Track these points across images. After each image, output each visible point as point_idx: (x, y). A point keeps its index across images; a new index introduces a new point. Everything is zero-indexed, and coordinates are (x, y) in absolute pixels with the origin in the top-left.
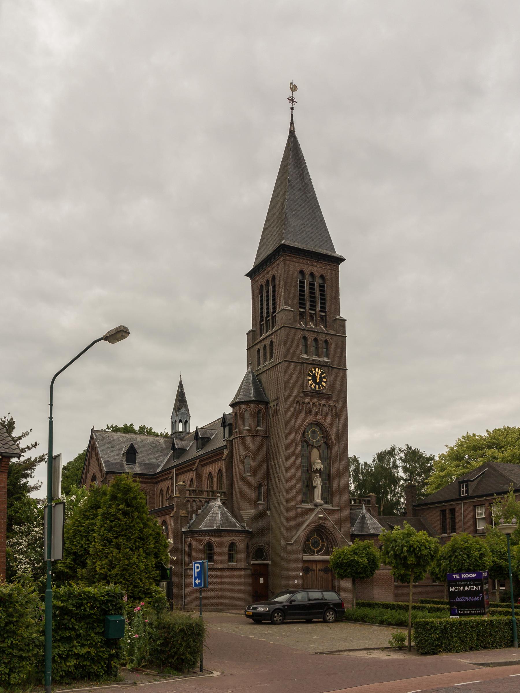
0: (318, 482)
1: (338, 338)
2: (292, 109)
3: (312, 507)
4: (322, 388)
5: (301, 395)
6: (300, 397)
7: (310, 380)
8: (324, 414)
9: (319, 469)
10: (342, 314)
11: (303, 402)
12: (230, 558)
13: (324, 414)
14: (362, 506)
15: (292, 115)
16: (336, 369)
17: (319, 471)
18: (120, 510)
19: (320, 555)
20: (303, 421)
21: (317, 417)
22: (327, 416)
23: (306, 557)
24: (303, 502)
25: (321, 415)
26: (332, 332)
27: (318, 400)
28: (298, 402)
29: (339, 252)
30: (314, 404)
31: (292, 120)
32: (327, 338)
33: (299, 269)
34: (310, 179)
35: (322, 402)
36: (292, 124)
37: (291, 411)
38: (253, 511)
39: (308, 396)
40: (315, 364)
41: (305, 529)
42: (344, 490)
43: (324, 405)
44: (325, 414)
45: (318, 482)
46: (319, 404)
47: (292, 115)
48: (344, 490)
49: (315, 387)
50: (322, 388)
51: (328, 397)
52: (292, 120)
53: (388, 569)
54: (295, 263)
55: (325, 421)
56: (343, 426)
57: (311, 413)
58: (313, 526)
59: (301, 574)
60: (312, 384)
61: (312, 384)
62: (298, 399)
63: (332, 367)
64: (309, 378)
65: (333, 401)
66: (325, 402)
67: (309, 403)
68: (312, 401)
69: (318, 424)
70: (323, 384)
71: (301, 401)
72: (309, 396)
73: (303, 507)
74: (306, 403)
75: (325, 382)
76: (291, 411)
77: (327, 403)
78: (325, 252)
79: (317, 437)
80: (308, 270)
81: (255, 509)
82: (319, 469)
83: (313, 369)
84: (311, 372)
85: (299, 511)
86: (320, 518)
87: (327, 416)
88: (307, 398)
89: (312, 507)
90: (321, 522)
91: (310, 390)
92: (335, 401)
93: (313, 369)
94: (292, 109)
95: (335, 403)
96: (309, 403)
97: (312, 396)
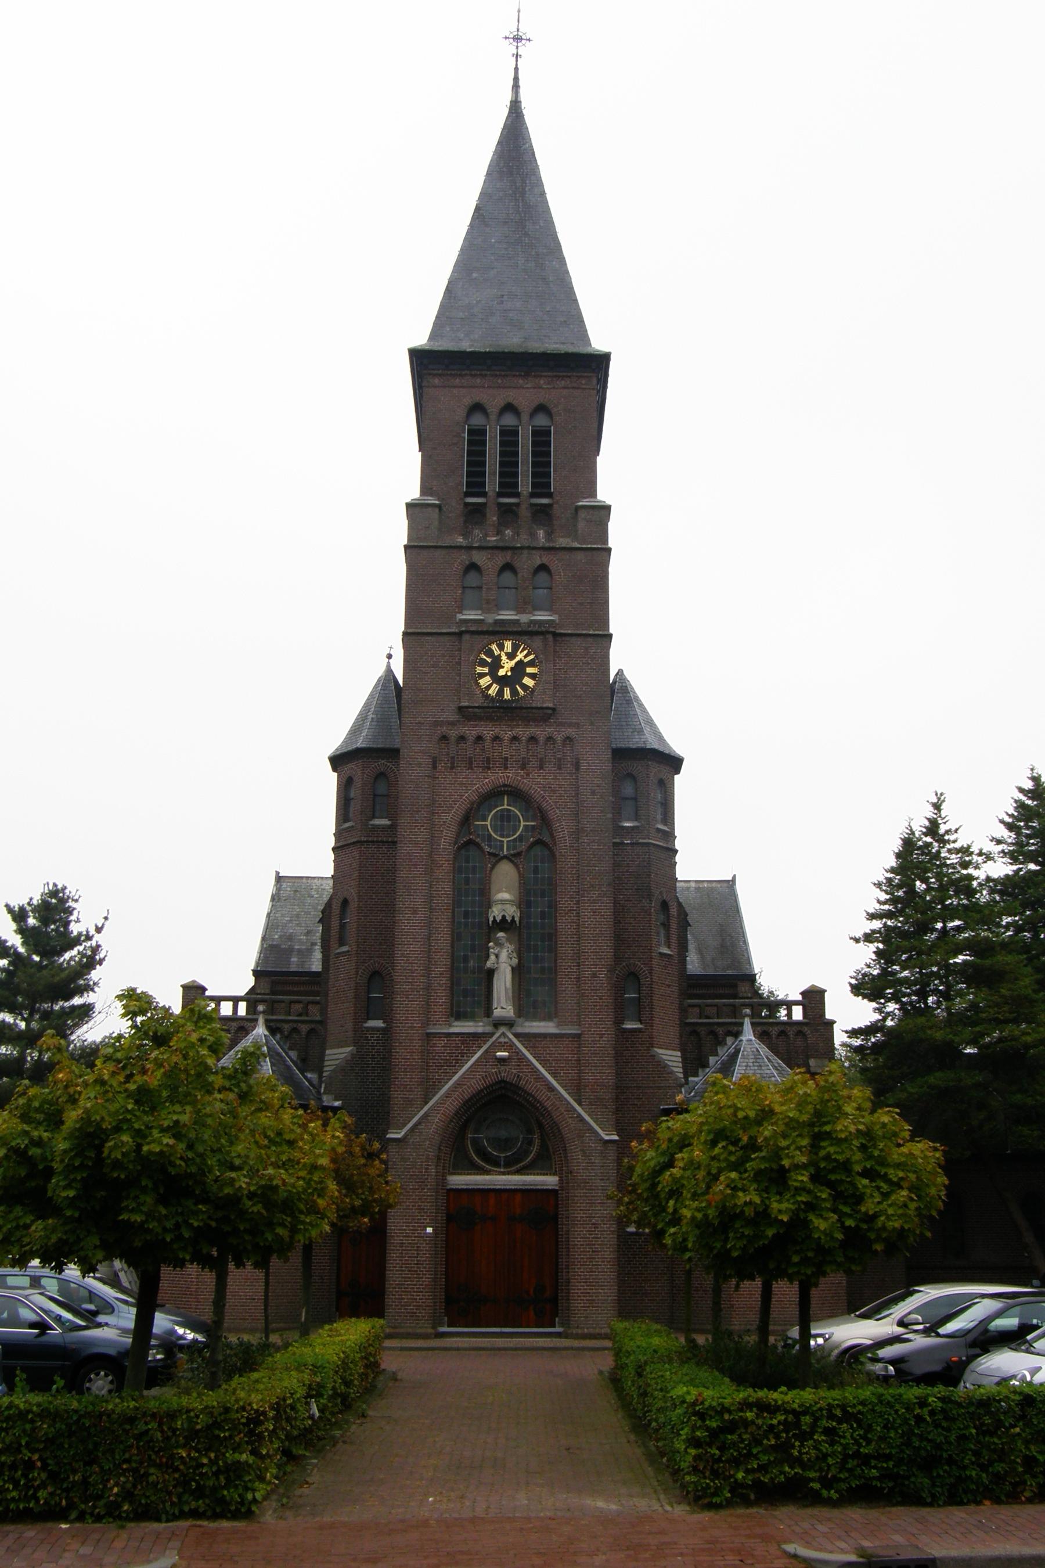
0: (503, 959)
1: (580, 556)
2: (517, 56)
3: (489, 1029)
4: (522, 692)
5: (454, 717)
6: (453, 724)
7: (482, 675)
8: (534, 763)
9: (498, 919)
10: (604, 493)
11: (462, 738)
13: (534, 763)
14: (256, 1020)
15: (516, 69)
16: (573, 639)
17: (504, 924)
19: (518, 1172)
20: (465, 786)
22: (541, 768)
23: (460, 1180)
24: (459, 1015)
26: (563, 542)
27: (512, 728)
28: (444, 738)
29: (598, 343)
30: (496, 738)
31: (516, 79)
32: (545, 560)
33: (468, 401)
34: (543, 194)
35: (523, 732)
36: (516, 86)
37: (419, 765)
38: (349, 1049)
40: (501, 632)
41: (447, 1095)
43: (533, 739)
44: (536, 764)
45: (503, 959)
46: (515, 739)
47: (516, 69)
48: (594, 975)
49: (500, 692)
50: (522, 692)
51: (546, 715)
52: (516, 79)
54: (455, 391)
55: (534, 783)
56: (593, 793)
57: (487, 765)
58: (476, 1084)
59: (429, 1230)
60: (489, 687)
61: (489, 687)
63: (555, 635)
64: (479, 670)
65: (562, 724)
66: (533, 730)
67: (479, 738)
68: (488, 731)
69: (516, 794)
70: (528, 682)
71: (453, 734)
72: (481, 719)
73: (527, 1030)
75: (532, 676)
76: (419, 765)
77: (541, 732)
78: (553, 344)
80: (494, 400)
81: (355, 1043)
82: (509, 919)
83: (494, 647)
84: (490, 653)
85: (440, 1044)
86: (502, 1060)
87: (541, 768)
88: (476, 726)
89: (489, 1029)
90: (509, 1073)
91: (479, 701)
92: (571, 725)
93: (494, 647)
94: (517, 56)
95: (571, 732)
96: (479, 738)
97: (490, 719)
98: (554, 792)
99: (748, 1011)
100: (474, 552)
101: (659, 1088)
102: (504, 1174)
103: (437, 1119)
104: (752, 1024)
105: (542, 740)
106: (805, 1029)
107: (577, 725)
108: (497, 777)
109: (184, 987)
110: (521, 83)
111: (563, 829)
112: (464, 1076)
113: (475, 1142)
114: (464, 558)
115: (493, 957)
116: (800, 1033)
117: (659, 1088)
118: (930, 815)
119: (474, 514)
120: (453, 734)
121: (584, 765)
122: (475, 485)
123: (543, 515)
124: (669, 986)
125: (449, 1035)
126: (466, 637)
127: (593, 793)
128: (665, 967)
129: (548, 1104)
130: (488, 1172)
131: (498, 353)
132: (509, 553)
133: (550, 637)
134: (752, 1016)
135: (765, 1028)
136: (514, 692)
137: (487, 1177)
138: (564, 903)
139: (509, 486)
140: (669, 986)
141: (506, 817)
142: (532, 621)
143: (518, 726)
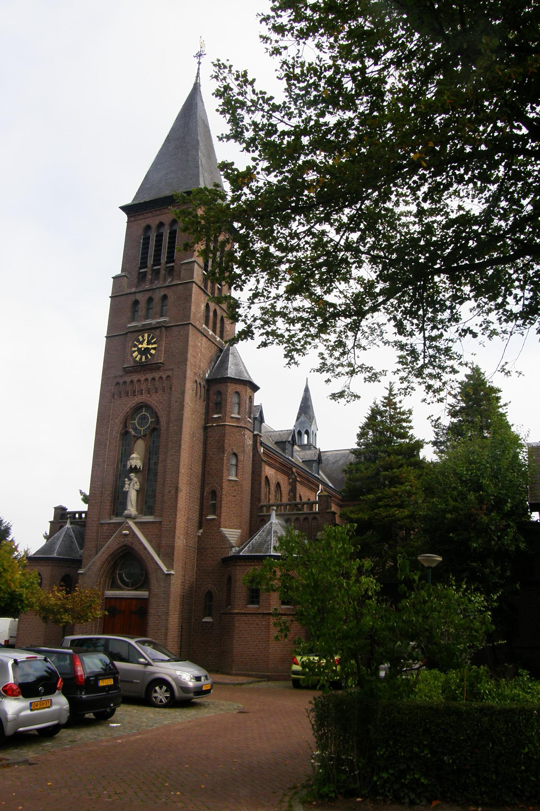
1: (181, 287)
2: (199, 63)
6: (121, 376)
7: (134, 352)
9: (133, 467)
12: (252, 597)
15: (199, 69)
16: (174, 328)
17: (135, 470)
18: (385, 556)
19: (136, 590)
21: (144, 397)
22: (156, 392)
23: (110, 593)
25: (149, 393)
32: (166, 292)
35: (149, 376)
39: (131, 372)
42: (170, 492)
46: (146, 380)
47: (199, 69)
48: (170, 492)
51: (155, 367)
53: (263, 614)
55: (153, 400)
58: (115, 547)
62: (118, 380)
63: (166, 327)
65: (166, 370)
74: (128, 382)
77: (156, 375)
79: (147, 423)
82: (133, 467)
86: (126, 535)
87: (156, 392)
90: (129, 540)
91: (132, 364)
92: (170, 370)
94: (199, 63)
95: (169, 373)
98: (161, 403)
99: (275, 508)
100: (137, 294)
101: (222, 548)
102: (129, 590)
103: (98, 564)
104: (276, 515)
105: (157, 379)
106: (318, 516)
107: (172, 370)
108: (138, 399)
109: (55, 508)
110: (200, 76)
111: (163, 421)
112: (111, 545)
113: (120, 575)
114: (132, 298)
115: (127, 486)
116: (314, 518)
117: (222, 548)
118: (387, 395)
119: (142, 277)
120: (121, 381)
121: (173, 388)
122: (144, 264)
123: (171, 271)
124: (234, 496)
125: (109, 524)
126: (129, 335)
127: (176, 402)
128: (233, 487)
129: (143, 556)
130: (122, 589)
131: (157, 199)
132: (151, 292)
133: (163, 329)
134: (276, 511)
135: (297, 516)
136: (147, 358)
137: (121, 592)
138: (161, 457)
139: (157, 261)
140: (234, 496)
141: (144, 418)
142: (157, 322)
143: (147, 373)
